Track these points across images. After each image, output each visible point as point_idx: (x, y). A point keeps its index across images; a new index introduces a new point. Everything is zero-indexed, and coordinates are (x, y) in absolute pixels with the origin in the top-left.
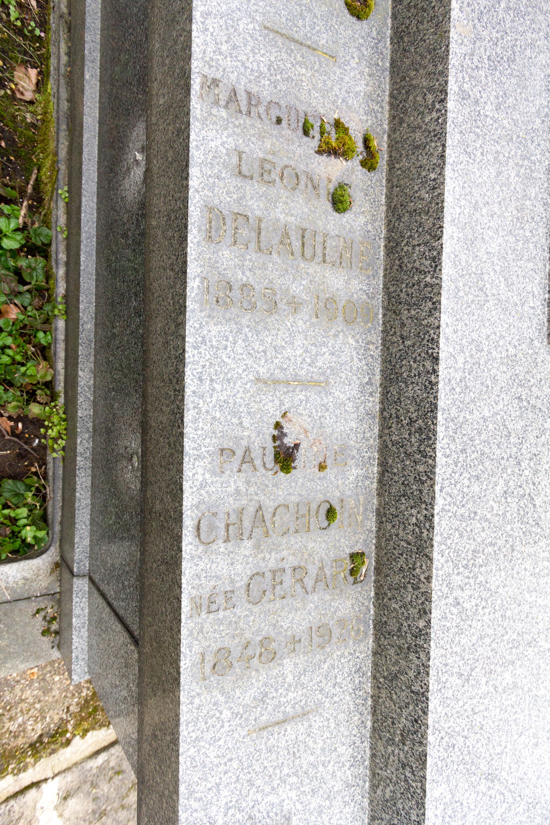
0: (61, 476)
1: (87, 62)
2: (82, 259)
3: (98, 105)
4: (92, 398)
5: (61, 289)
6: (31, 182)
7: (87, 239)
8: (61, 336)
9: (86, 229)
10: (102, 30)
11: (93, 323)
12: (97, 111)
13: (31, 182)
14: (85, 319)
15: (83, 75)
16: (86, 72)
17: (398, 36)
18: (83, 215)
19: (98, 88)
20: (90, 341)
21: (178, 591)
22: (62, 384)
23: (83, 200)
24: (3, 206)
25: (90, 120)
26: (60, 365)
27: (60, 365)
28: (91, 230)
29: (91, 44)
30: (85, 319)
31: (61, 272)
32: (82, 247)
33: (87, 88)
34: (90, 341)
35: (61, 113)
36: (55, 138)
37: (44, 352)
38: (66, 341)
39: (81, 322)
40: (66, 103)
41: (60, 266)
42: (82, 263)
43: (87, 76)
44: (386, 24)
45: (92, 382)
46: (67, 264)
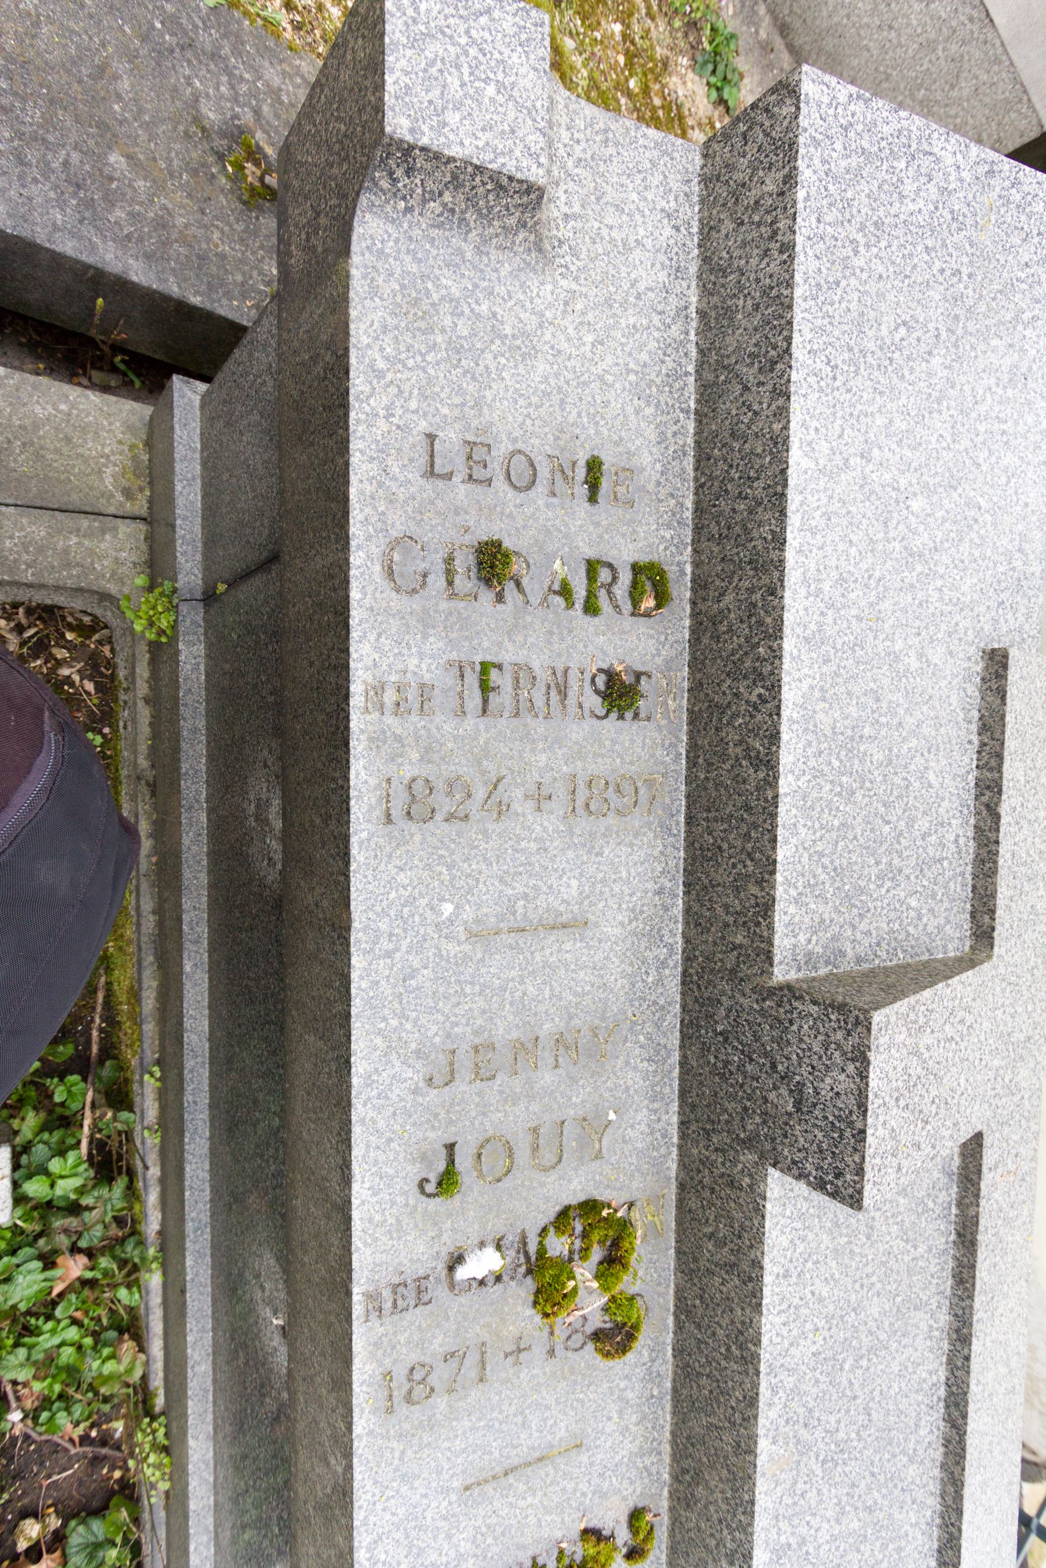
0: (164, 1520)
1: (187, 945)
2: (189, 1262)
3: (207, 1012)
4: (212, 1479)
5: (153, 1224)
6: (99, 1009)
7: (195, 1231)
8: (156, 1299)
9: (194, 1215)
10: (211, 886)
11: (210, 1362)
12: (207, 1023)
13: (99, 1009)
14: (196, 1357)
15: (181, 966)
16: (185, 962)
17: (685, 1371)
18: (187, 1194)
19: (206, 985)
20: (206, 1391)
21: (754, 776)
22: (161, 1374)
23: (188, 1169)
24: (3, 509)
25: (194, 1038)
26: (156, 1347)
27: (156, 1347)
28: (202, 1216)
29: (192, 914)
30: (196, 1357)
31: (153, 1197)
32: (188, 1244)
33: (188, 986)
34: (206, 1391)
35: (144, 939)
36: (134, 920)
37: (130, 1327)
38: (165, 1303)
39: (190, 1363)
40: (151, 918)
41: (151, 1190)
42: (188, 1270)
43: (188, 968)
44: (666, 1326)
45: (211, 1454)
46: (163, 1181)
